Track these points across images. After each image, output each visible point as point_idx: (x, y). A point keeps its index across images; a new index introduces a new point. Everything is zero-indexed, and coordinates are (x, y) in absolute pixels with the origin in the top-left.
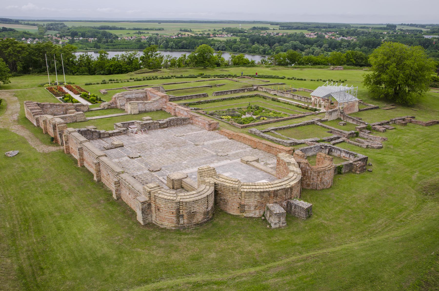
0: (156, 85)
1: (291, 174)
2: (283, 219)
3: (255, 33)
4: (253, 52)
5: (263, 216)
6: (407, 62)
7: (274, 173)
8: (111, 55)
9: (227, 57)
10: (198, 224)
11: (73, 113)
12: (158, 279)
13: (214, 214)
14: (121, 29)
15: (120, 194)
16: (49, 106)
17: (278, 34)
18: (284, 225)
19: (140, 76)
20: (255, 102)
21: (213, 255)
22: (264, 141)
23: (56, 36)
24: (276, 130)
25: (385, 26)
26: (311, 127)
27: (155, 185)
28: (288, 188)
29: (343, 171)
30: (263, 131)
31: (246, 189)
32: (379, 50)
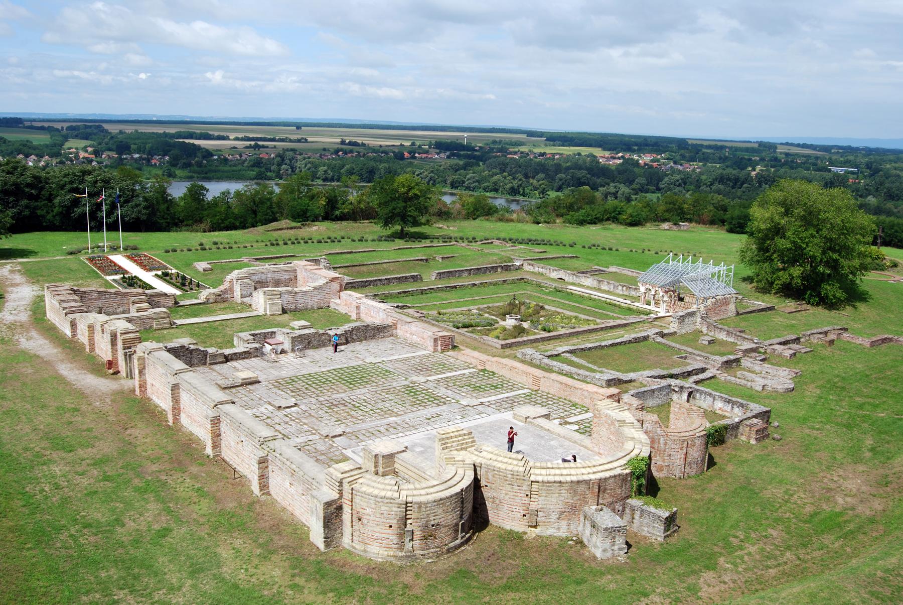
8: (214, 190)
9: (636, 148)
16: (95, 295)
23: (87, 151)
25: (756, 146)
27: (352, 467)
28: (627, 474)
30: (546, 354)
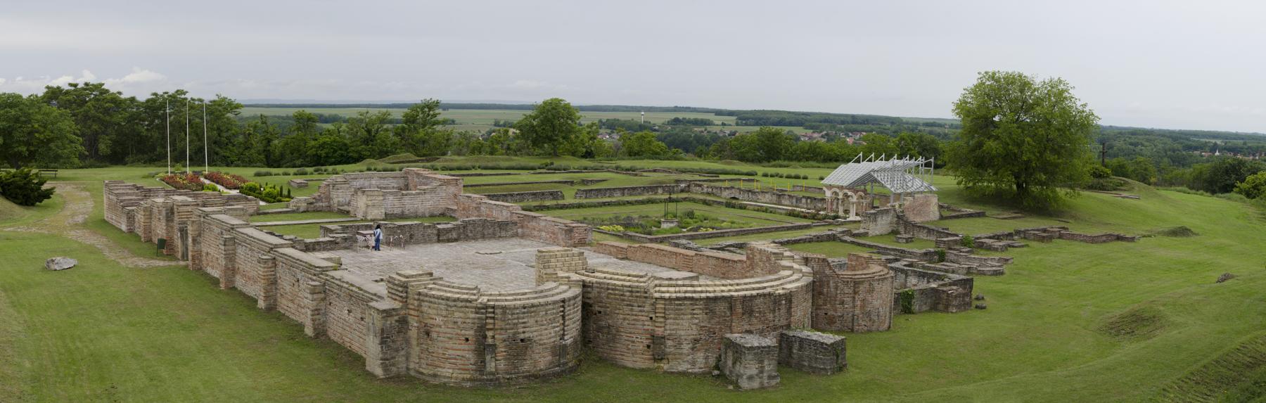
5: (717, 367)
10: (536, 377)
13: (580, 361)
15: (324, 324)
17: (733, 134)
18: (773, 382)
29: (916, 307)
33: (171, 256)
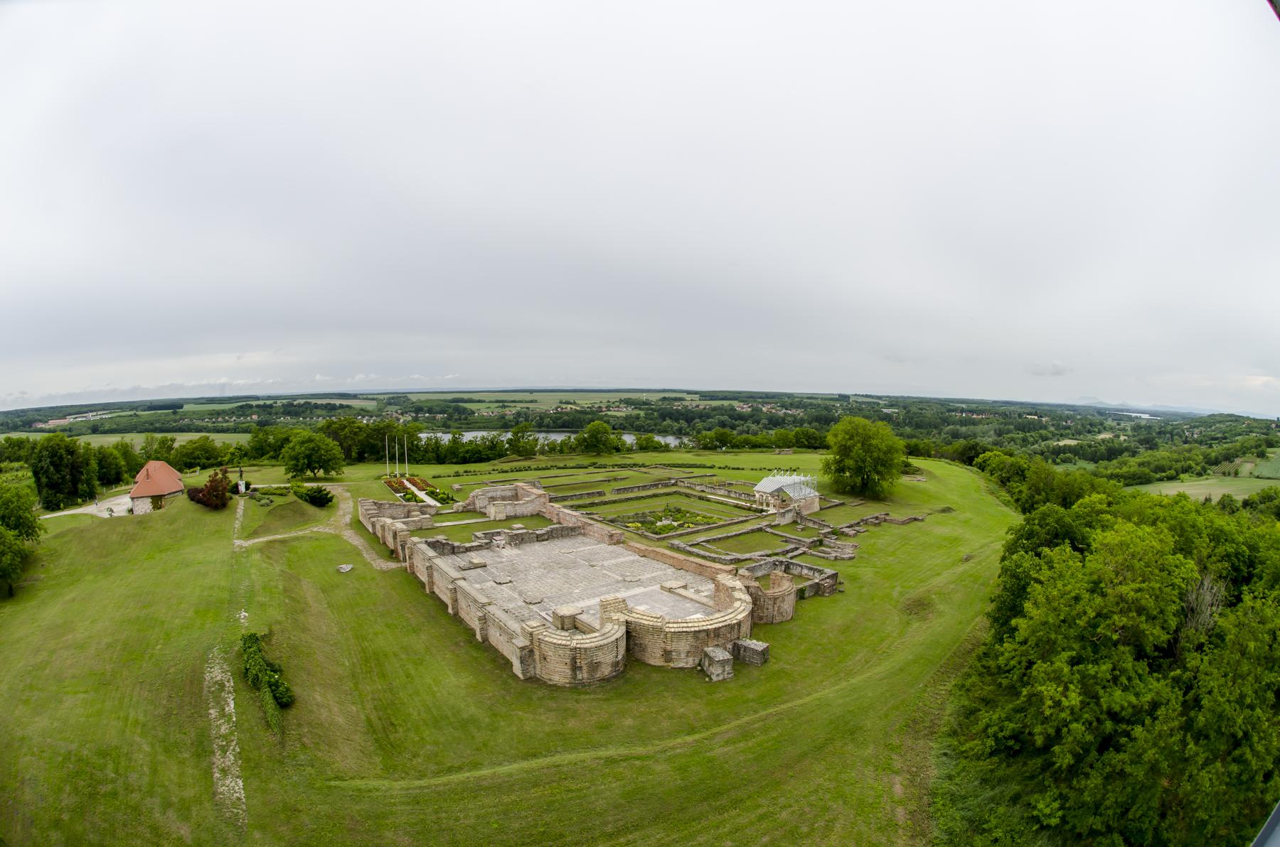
0: (530, 479)
1: (737, 604)
2: (728, 668)
3: (665, 405)
4: (664, 432)
6: (874, 442)
7: (711, 603)
8: (468, 437)
9: (629, 439)
11: (417, 517)
12: (550, 752)
14: (479, 401)
19: (506, 466)
20: (675, 502)
21: (629, 722)
22: (692, 559)
24: (708, 541)
26: (757, 535)
31: (673, 628)
32: (839, 427)
33: (397, 559)
